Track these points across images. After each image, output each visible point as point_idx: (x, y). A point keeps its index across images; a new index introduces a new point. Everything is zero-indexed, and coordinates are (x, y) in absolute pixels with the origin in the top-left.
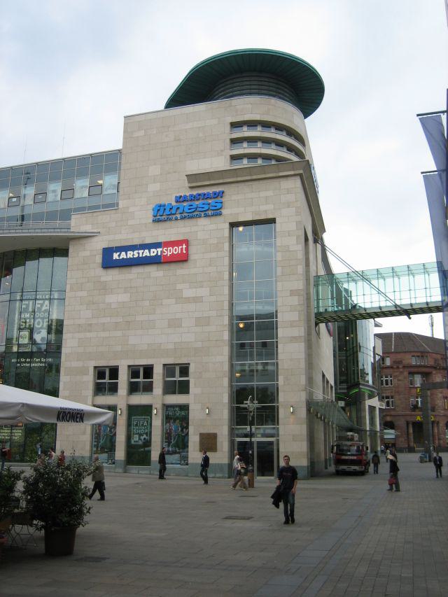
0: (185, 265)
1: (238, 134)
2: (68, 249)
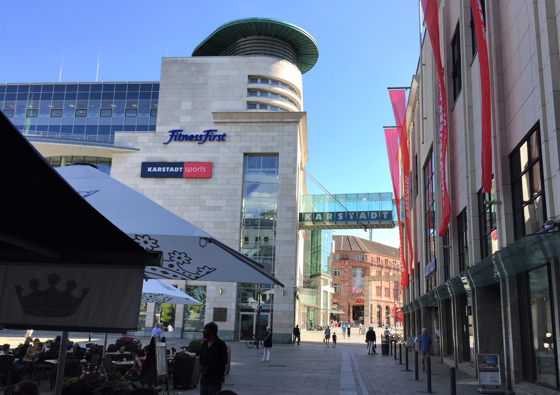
0: (209, 181)
1: (253, 86)
2: (155, 126)
